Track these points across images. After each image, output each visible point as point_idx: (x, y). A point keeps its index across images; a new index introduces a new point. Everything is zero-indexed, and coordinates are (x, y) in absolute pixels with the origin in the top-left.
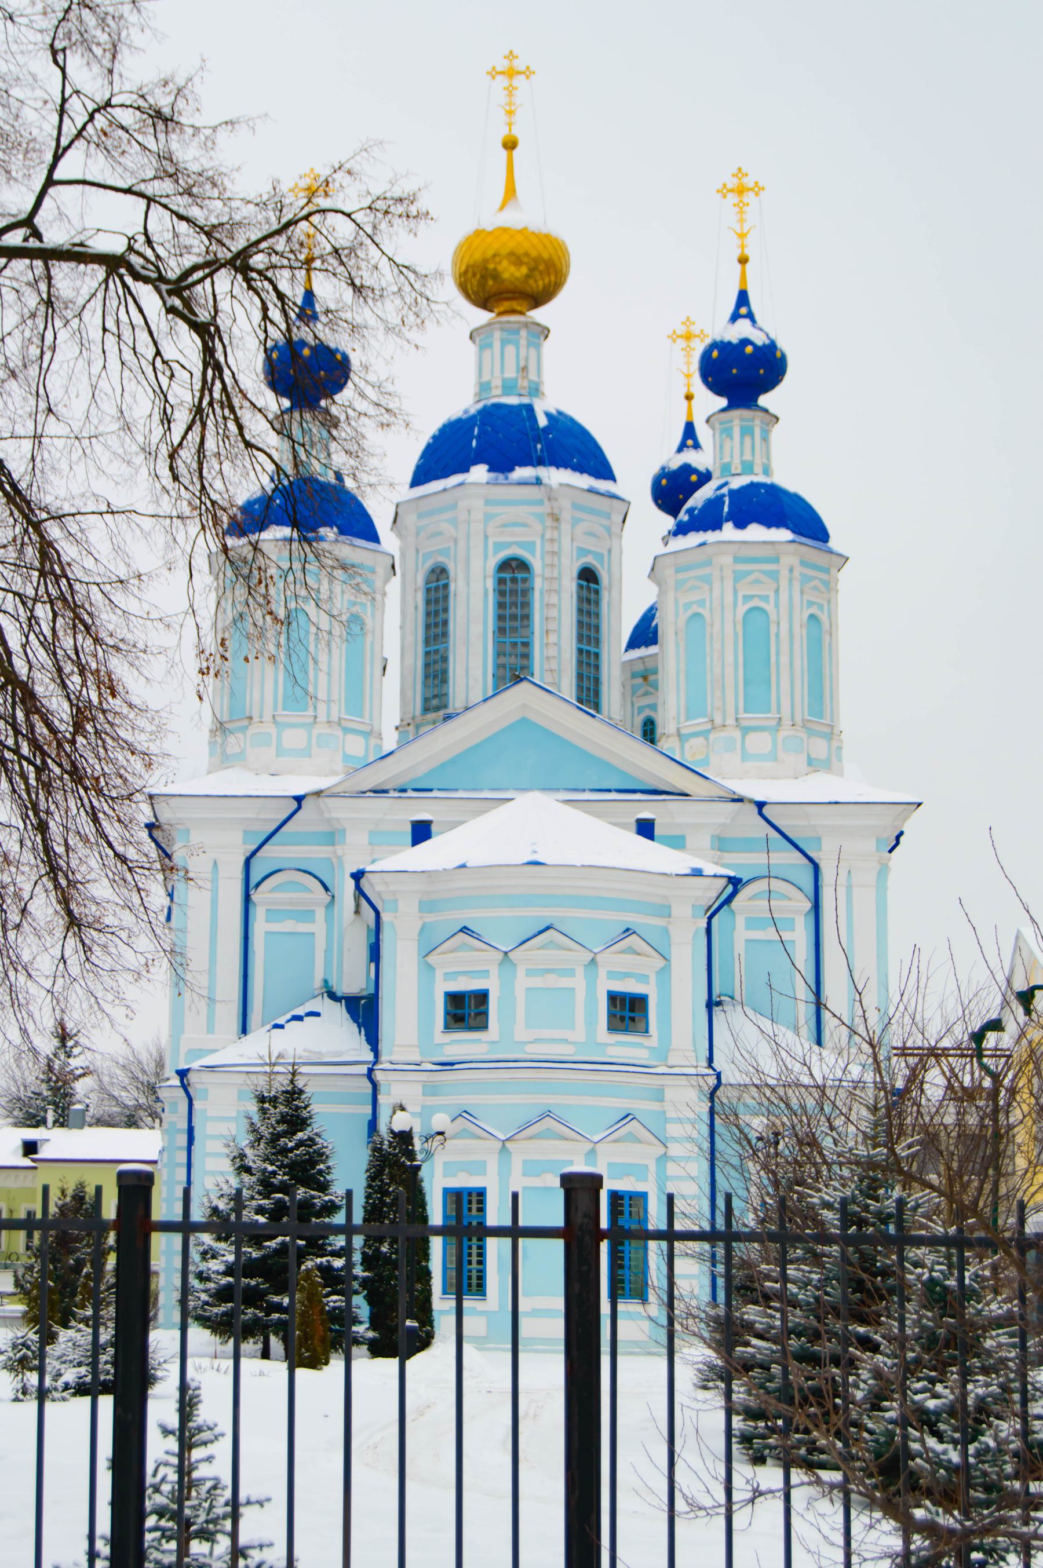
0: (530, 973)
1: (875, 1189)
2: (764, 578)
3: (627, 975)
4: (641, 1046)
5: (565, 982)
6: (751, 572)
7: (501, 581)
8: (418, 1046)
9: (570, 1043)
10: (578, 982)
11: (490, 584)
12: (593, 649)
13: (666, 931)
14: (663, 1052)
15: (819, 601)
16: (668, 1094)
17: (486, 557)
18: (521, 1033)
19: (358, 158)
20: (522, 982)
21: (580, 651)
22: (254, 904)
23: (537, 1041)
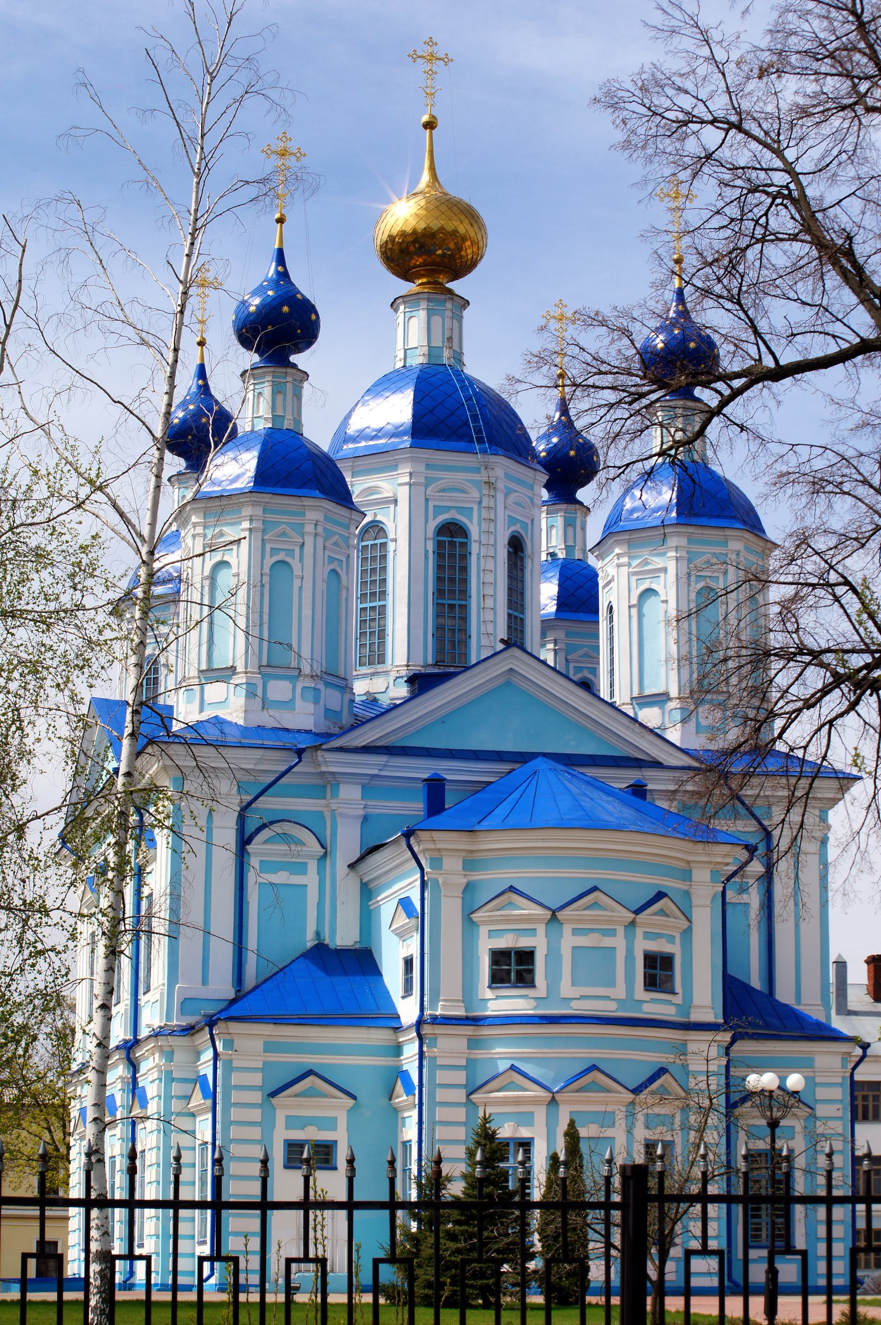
0: (575, 932)
1: (489, 1135)
2: (288, 530)
3: (658, 936)
4: (669, 1002)
5: (608, 942)
6: (705, 553)
7: (440, 545)
8: (463, 1001)
9: (613, 1000)
10: (619, 942)
11: (430, 546)
12: (521, 616)
13: (687, 894)
14: (687, 1005)
15: (338, 557)
16: (691, 1047)
17: (427, 521)
18: (566, 989)
19: (279, 107)
20: (568, 941)
21: (510, 615)
22: (248, 853)
23: (582, 997)
